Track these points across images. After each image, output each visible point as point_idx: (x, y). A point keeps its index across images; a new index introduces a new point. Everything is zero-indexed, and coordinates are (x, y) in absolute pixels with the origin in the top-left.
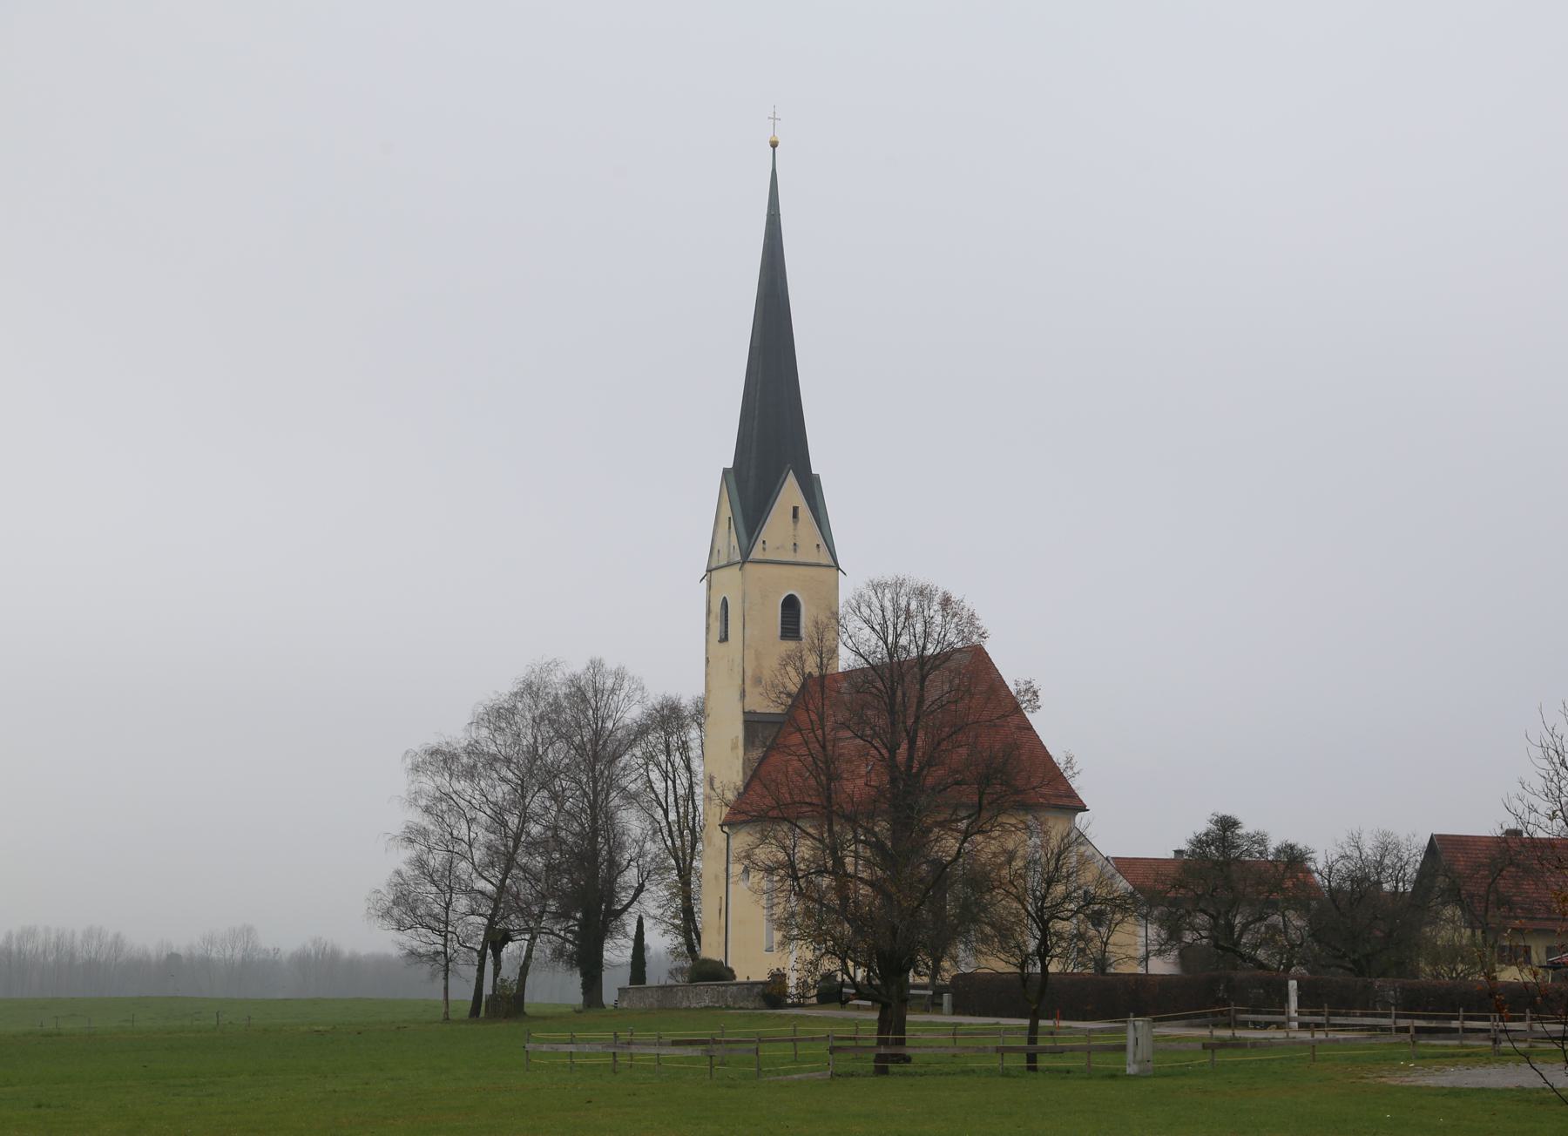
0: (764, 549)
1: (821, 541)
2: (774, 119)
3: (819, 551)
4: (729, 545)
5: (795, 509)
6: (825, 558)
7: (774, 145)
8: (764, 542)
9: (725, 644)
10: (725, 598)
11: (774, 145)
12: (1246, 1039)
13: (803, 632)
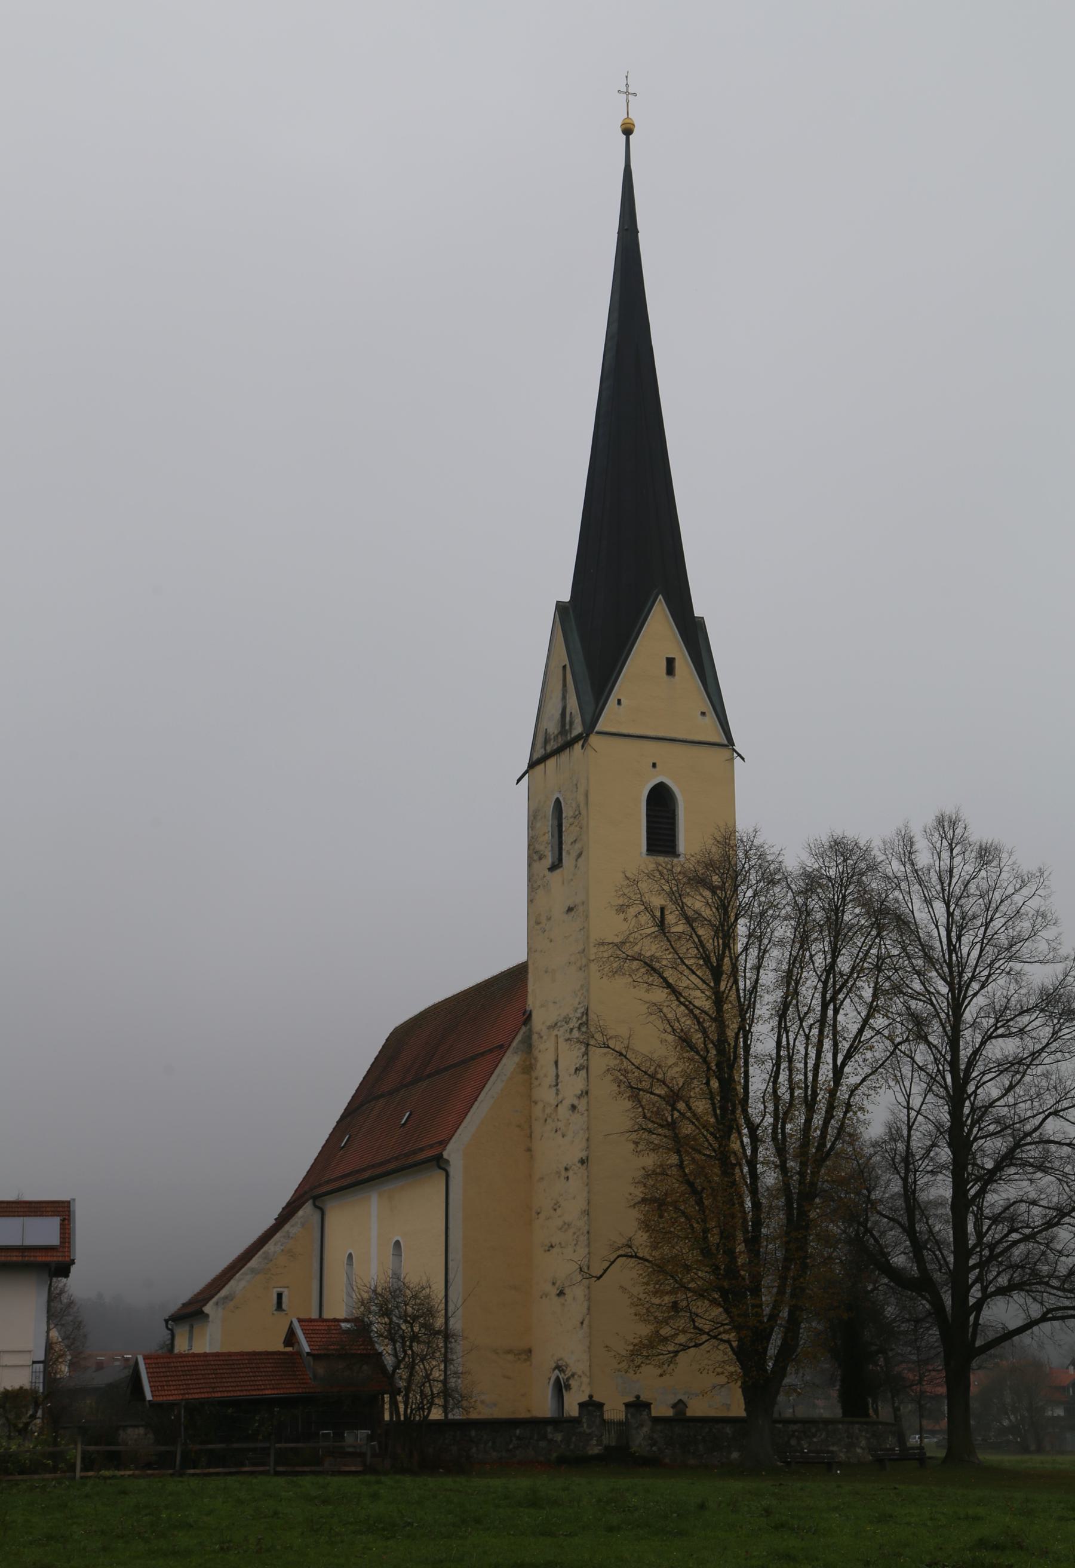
1: (708, 707)
2: (627, 93)
5: (670, 663)
6: (710, 731)
7: (628, 131)
10: (558, 801)
11: (628, 131)
12: (298, 1343)
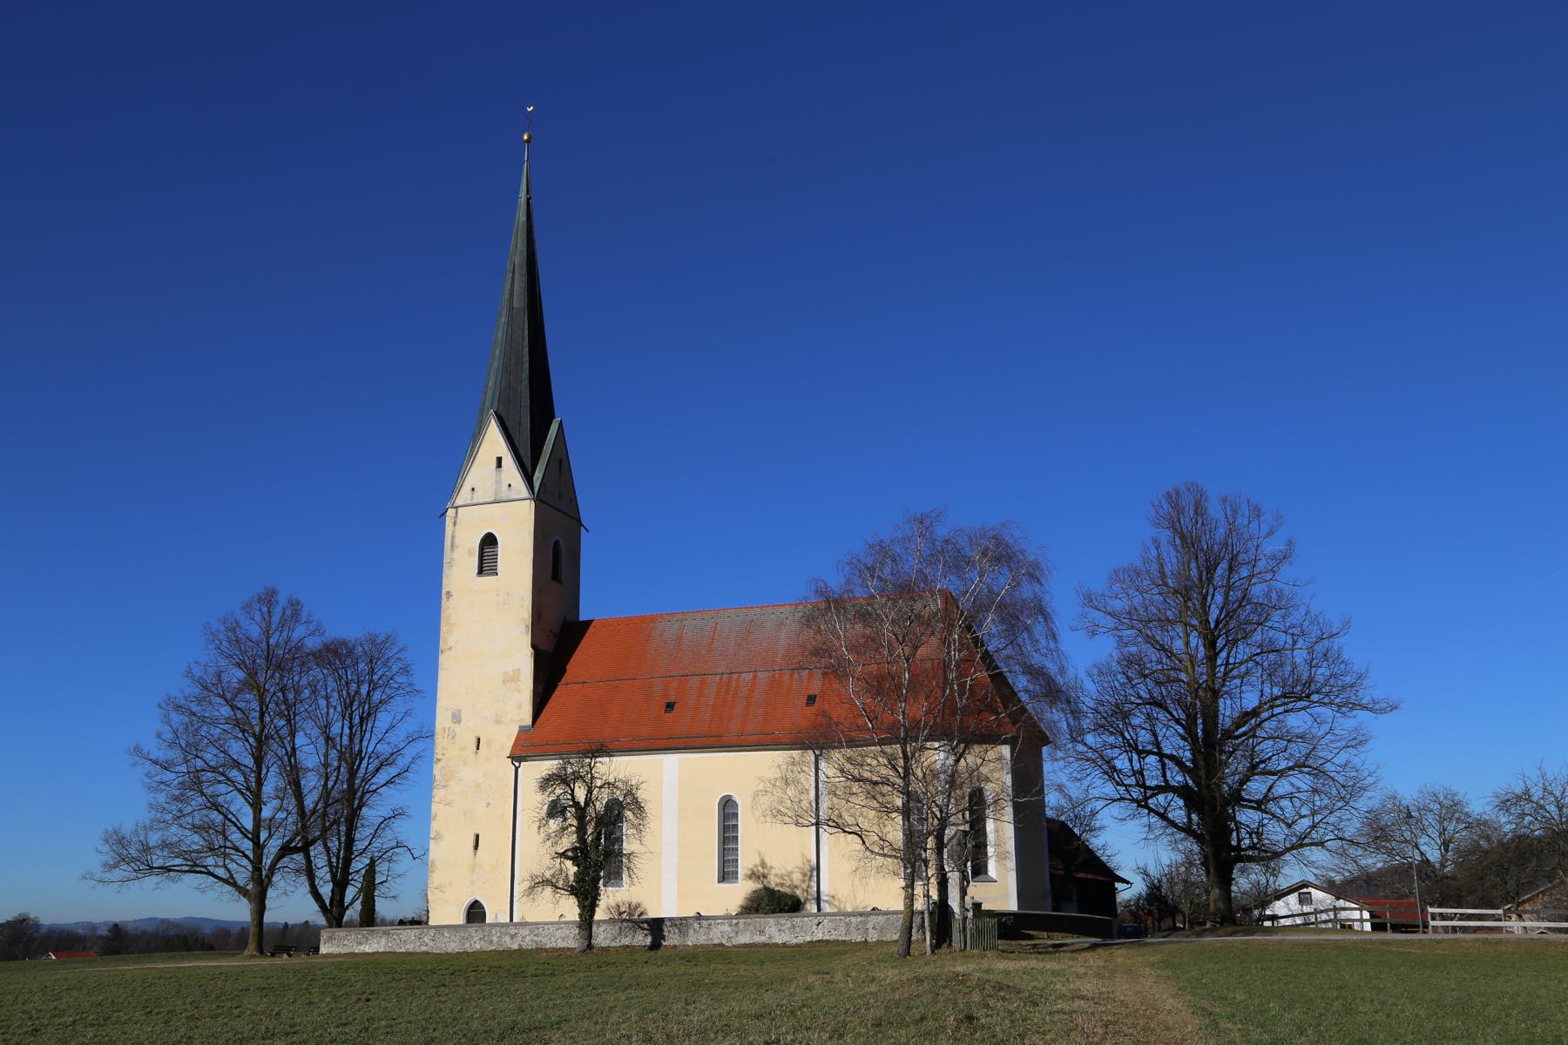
4: (498, 482)
5: (499, 460)
9: (487, 580)
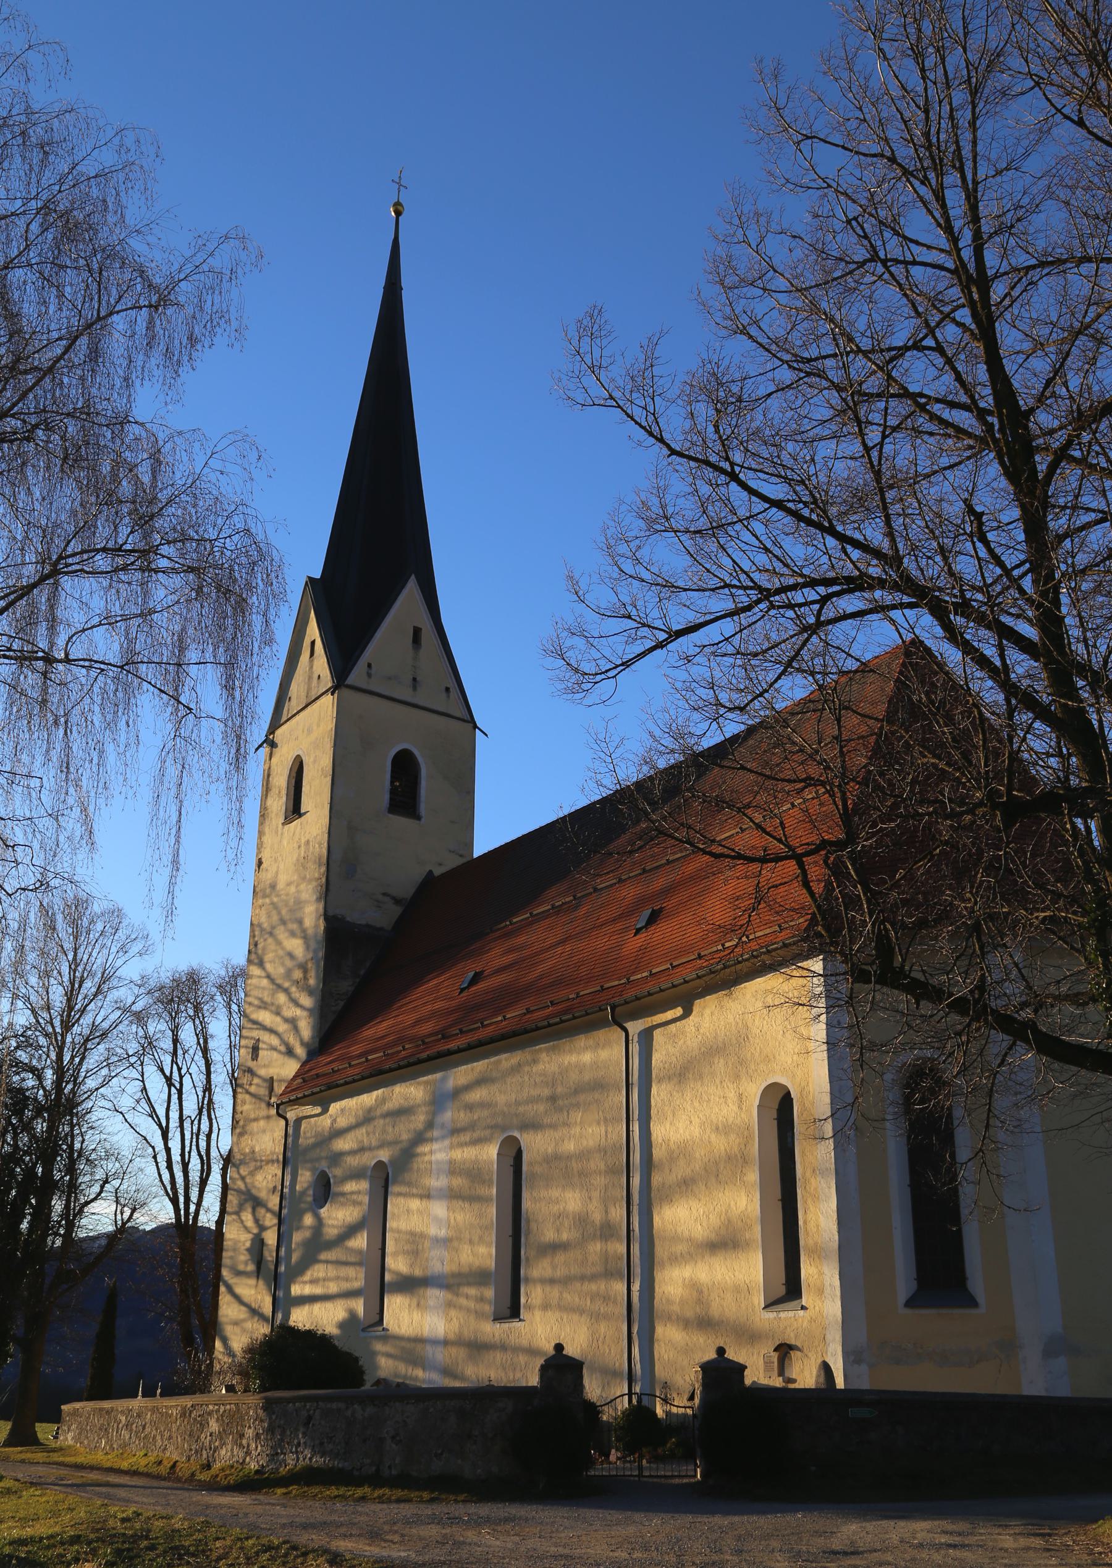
0: (369, 675)
3: (448, 697)
5: (417, 632)
8: (369, 666)
13: (423, 808)
